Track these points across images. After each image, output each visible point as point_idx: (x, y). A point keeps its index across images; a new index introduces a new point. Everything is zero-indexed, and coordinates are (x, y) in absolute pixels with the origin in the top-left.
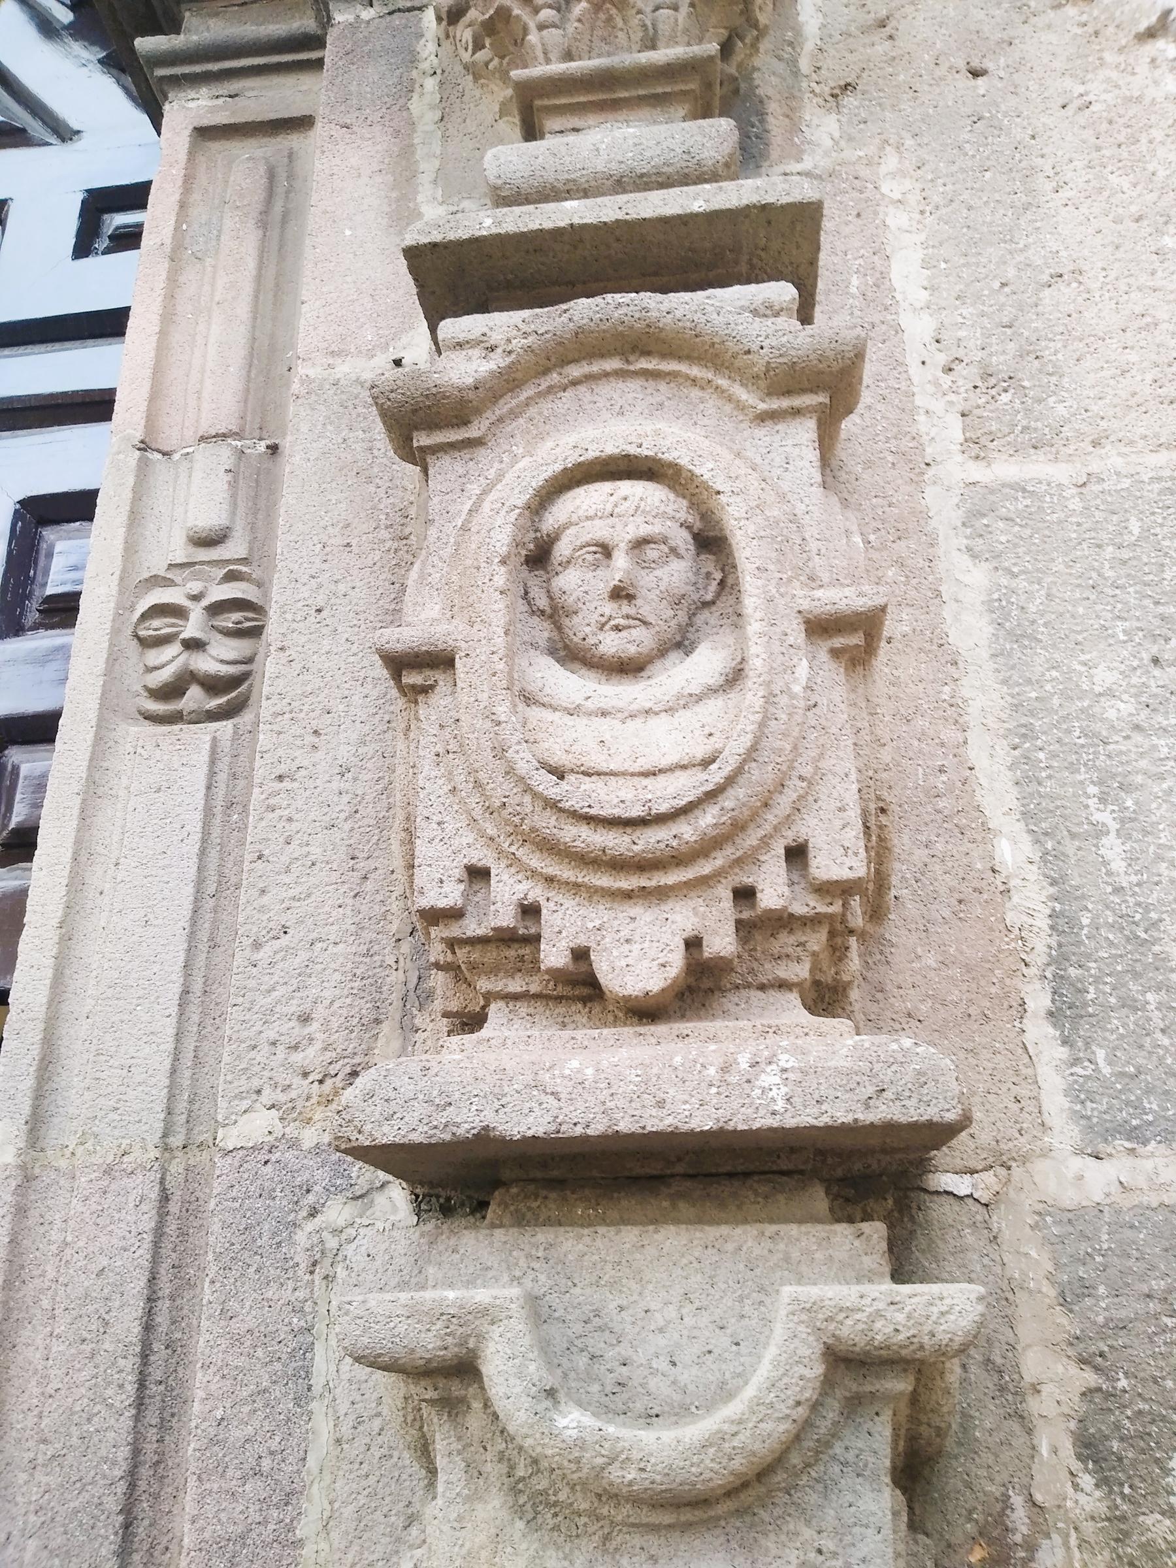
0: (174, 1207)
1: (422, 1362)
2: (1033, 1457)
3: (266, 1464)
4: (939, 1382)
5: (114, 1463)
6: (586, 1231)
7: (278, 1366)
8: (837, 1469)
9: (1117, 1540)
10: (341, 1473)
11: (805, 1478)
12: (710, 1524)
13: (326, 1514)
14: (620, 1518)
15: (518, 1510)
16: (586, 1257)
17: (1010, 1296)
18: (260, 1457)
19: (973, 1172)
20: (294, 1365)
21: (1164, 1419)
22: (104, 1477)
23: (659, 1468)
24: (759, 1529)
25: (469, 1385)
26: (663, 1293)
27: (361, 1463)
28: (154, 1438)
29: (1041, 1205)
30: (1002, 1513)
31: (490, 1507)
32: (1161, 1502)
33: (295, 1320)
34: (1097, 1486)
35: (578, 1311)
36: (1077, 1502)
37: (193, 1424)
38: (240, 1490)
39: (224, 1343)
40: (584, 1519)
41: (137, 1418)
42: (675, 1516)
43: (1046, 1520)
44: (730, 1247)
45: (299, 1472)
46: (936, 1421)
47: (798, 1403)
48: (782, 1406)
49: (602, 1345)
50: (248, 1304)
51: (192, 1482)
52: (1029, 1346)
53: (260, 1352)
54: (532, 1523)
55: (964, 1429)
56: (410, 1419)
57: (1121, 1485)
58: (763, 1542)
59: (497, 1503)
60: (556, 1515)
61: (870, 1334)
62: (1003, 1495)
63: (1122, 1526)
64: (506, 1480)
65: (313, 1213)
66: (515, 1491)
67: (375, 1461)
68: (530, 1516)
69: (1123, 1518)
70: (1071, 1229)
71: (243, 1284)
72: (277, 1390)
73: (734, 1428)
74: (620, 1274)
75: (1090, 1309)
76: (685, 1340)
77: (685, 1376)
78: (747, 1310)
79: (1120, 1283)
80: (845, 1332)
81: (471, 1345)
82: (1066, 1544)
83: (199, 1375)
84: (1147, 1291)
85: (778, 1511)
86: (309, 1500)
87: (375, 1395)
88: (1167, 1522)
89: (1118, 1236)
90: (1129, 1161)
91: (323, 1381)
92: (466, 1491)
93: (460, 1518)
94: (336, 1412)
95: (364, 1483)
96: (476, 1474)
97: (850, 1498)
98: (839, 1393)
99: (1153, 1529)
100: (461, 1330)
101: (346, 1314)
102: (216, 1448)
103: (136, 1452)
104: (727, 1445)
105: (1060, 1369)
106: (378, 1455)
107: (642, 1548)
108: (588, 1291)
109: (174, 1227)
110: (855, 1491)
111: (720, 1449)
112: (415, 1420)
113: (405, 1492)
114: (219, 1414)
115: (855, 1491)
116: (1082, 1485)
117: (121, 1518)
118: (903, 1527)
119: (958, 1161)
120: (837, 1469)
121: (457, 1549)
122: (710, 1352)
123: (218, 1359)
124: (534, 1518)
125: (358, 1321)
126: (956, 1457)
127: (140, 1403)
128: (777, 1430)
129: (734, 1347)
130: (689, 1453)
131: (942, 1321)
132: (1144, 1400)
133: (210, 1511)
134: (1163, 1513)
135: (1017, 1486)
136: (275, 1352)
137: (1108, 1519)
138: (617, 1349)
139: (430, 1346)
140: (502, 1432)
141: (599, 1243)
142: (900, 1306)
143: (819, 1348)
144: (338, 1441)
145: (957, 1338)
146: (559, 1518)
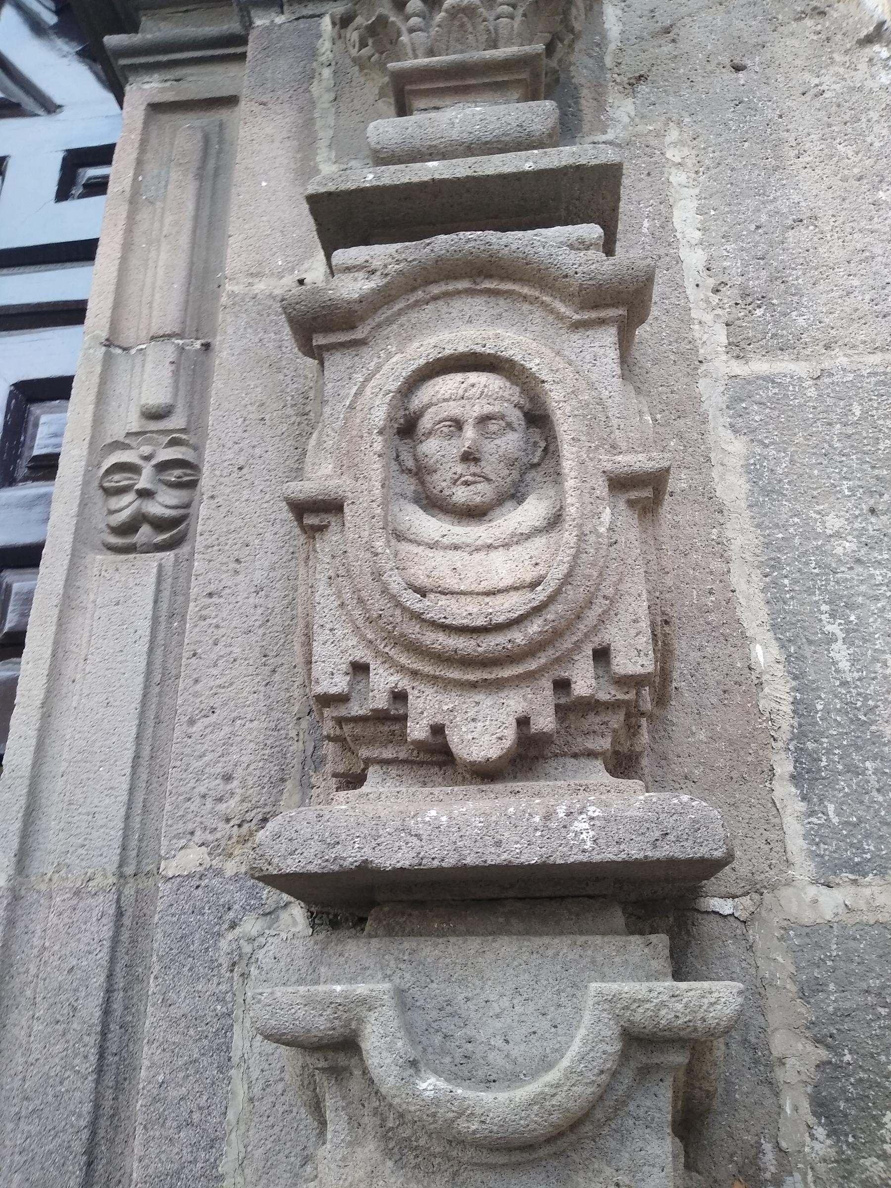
0: (127, 921)
1: (316, 1039)
2: (779, 1114)
3: (196, 1116)
4: (708, 1056)
5: (80, 1116)
6: (441, 940)
7: (205, 1042)
8: (631, 1122)
9: (844, 1177)
10: (253, 1124)
11: (606, 1129)
12: (535, 1163)
13: (242, 1155)
14: (466, 1159)
15: (388, 1153)
16: (441, 961)
17: (762, 990)
18: (191, 1112)
19: (734, 897)
20: (217, 1041)
21: (878, 1085)
22: (72, 1126)
23: (496, 1121)
24: (571, 1168)
25: (352, 1057)
26: (499, 988)
27: (268, 1117)
28: (111, 1097)
29: (786, 922)
30: (756, 1157)
31: (366, 1150)
32: (877, 1148)
33: (219, 1007)
34: (828, 1136)
35: (434, 1001)
36: (812, 1148)
37: (141, 1086)
38: (176, 1136)
39: (164, 1024)
40: (438, 1160)
41: (98, 1082)
42: (507, 1157)
43: (789, 1161)
44: (550, 953)
45: (221, 1123)
46: (706, 1086)
47: (602, 1072)
48: (590, 1074)
49: (453, 1027)
50: (183, 995)
51: (140, 1130)
52: (776, 1029)
53: (192, 1032)
54: (399, 1163)
55: (727, 1092)
56: (306, 1083)
57: (847, 1135)
58: (574, 1177)
59: (372, 1147)
60: (417, 1156)
61: (656, 1019)
62: (756, 1142)
63: (847, 1167)
64: (379, 1130)
65: (233, 926)
66: (386, 1138)
67: (279, 1115)
68: (397, 1157)
69: (848, 1161)
70: (808, 941)
71: (180, 979)
72: (205, 1061)
73: (553, 1091)
74: (467, 973)
75: (822, 1001)
76: (515, 1024)
77: (516, 1051)
78: (563, 1000)
79: (846, 982)
80: (637, 1017)
81: (353, 1027)
82: (804, 1180)
83: (146, 1049)
84: (866, 988)
85: (585, 1154)
86: (229, 1145)
87: (279, 1065)
88: (882, 1164)
89: (844, 946)
90: (852, 889)
91: (239, 1053)
92: (349, 1138)
93: (344, 1159)
94: (249, 1077)
95: (271, 1132)
96: (356, 1125)
97: (640, 1144)
98: (633, 1064)
99: (871, 1169)
100: (346, 1015)
101: (259, 1002)
102: (158, 1105)
103: (97, 1107)
104: (548, 1103)
105: (800, 1046)
106: (281, 1110)
107: (482, 1182)
108: (442, 986)
109: (127, 936)
110: (644, 1139)
111: (542, 1107)
112: (310, 1083)
113: (302, 1139)
114: (160, 1078)
115: (644, 1139)
116: (817, 1135)
117: (85, 1158)
118: (681, 1166)
119: (723, 888)
120: (631, 1122)
121: (341, 1182)
122: (534, 1033)
123: (159, 1036)
124: (401, 1159)
125: (267, 1008)
126: (721, 1113)
127: (100, 1071)
128: (585, 1092)
129: (553, 1030)
130: (519, 1110)
131: (711, 1009)
132: (864, 1071)
133: (153, 1151)
134: (878, 1157)
135: (767, 1136)
136: (203, 1031)
137: (836, 1161)
138: (464, 1030)
139: (322, 1028)
140: (376, 1093)
141: (450, 949)
142: (680, 998)
143: (617, 1030)
144: (251, 1100)
145: (722, 1023)
146: (419, 1159)
